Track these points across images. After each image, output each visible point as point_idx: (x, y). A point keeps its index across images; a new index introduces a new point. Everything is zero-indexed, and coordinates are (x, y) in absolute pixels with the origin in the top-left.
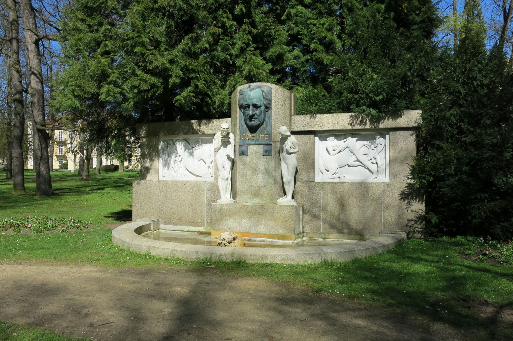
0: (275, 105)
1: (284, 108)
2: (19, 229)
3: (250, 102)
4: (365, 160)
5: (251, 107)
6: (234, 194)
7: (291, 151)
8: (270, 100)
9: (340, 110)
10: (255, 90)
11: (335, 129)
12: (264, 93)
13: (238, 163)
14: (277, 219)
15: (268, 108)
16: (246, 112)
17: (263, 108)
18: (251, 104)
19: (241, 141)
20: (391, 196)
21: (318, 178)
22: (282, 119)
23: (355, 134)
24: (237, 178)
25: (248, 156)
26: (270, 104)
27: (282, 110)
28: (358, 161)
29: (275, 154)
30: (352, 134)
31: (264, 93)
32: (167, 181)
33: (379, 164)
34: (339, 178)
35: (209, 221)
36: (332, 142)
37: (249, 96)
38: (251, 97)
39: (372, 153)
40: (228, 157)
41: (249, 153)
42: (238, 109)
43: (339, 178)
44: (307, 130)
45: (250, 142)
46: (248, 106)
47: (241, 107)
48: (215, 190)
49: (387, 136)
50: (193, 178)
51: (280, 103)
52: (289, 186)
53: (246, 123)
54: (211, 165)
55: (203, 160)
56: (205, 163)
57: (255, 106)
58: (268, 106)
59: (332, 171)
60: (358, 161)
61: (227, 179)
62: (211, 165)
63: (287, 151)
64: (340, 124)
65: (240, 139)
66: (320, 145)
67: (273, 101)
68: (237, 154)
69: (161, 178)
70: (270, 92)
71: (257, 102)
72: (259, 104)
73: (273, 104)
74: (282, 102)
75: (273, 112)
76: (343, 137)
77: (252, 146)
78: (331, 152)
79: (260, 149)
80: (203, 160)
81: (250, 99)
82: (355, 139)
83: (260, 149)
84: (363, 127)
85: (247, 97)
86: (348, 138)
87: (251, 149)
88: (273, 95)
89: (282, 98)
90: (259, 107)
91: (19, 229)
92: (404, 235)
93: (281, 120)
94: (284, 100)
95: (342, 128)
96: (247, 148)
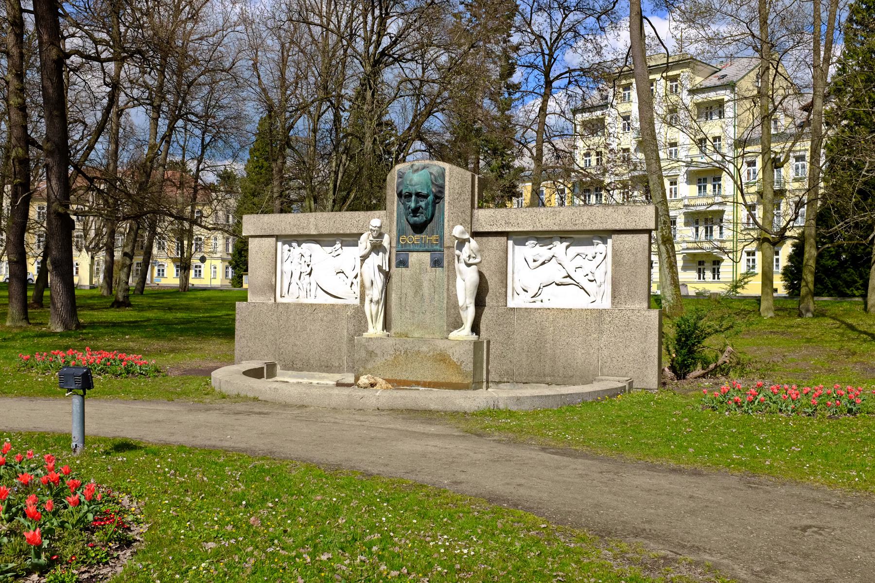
3: (412, 189)
4: (578, 276)
6: (386, 325)
11: (535, 229)
13: (394, 279)
15: (438, 197)
18: (414, 192)
19: (400, 246)
20: (612, 329)
23: (566, 238)
27: (459, 202)
28: (569, 276)
29: (448, 265)
30: (561, 238)
31: (432, 176)
32: (289, 304)
34: (542, 301)
36: (532, 250)
39: (589, 266)
40: (380, 268)
42: (396, 195)
43: (542, 301)
45: (412, 248)
47: (400, 195)
48: (360, 319)
49: (610, 241)
64: (543, 223)
65: (398, 242)
67: (447, 188)
68: (394, 263)
70: (443, 175)
71: (422, 189)
72: (425, 192)
73: (447, 192)
75: (446, 205)
76: (548, 241)
77: (415, 254)
79: (426, 257)
81: (411, 185)
82: (565, 244)
83: (426, 257)
86: (555, 243)
87: (413, 257)
88: (447, 179)
89: (460, 183)
92: (337, 364)
95: (545, 228)
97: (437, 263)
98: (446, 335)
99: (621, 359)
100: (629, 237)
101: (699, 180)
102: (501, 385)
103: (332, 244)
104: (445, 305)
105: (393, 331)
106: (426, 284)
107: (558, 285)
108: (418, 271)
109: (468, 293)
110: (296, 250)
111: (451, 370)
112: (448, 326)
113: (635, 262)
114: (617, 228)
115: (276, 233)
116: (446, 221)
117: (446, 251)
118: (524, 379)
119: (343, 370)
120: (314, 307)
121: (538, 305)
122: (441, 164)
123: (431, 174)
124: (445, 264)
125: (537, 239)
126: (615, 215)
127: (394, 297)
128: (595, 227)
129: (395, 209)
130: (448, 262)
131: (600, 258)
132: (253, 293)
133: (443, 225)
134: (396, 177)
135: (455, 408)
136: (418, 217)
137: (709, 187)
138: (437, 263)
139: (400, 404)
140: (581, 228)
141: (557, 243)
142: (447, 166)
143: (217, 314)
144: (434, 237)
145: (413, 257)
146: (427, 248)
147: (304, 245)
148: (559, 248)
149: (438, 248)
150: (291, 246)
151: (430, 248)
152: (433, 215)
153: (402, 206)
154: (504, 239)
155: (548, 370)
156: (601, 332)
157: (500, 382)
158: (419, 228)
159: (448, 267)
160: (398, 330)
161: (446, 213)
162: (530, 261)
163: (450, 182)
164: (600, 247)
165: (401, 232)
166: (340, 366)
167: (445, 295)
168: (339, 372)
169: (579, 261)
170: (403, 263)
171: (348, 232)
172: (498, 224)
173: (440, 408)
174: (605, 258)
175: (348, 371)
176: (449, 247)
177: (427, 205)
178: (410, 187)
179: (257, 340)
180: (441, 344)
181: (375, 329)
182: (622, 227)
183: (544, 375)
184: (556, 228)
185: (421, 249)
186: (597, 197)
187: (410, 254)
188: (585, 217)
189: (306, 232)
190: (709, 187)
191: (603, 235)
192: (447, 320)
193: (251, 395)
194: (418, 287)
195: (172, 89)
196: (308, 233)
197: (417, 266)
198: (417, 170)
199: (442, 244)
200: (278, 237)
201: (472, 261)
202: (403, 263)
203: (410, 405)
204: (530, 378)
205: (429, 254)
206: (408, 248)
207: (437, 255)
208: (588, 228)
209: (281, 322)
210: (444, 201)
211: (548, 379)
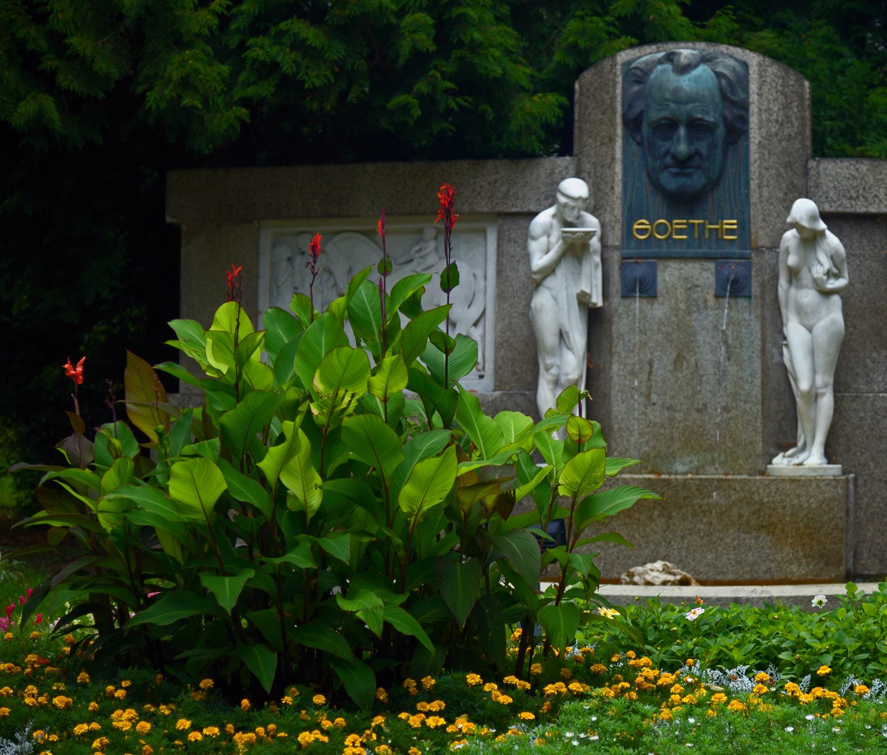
0: (761, 121)
1: (786, 133)
2: (625, 721)
5: (682, 131)
8: (744, 106)
9: (737, 42)
12: (723, 82)
13: (620, 326)
14: (780, 526)
16: (660, 143)
17: (721, 131)
22: (782, 170)
24: (615, 378)
25: (660, 299)
26: (745, 120)
27: (780, 141)
29: (763, 292)
31: (723, 82)
40: (583, 300)
41: (660, 287)
44: (863, 210)
45: (664, 250)
47: (632, 124)
51: (775, 116)
52: (565, 343)
53: (655, 184)
57: (696, 127)
58: (739, 125)
67: (753, 109)
70: (743, 81)
73: (754, 121)
74: (781, 113)
77: (673, 265)
81: (678, 102)
84: (754, 76)
85: (668, 95)
88: (753, 87)
89: (781, 99)
91: (625, 721)
93: (779, 175)
94: (786, 107)
96: (654, 268)
98: (760, 467)
108: (682, 306)
109: (821, 360)
111: (787, 549)
112: (765, 442)
116: (753, 185)
122: (738, 52)
123: (719, 75)
124: (755, 289)
129: (619, 155)
130: (762, 285)
133: (748, 196)
136: (689, 175)
142: (753, 59)
143: (609, 507)
144: (731, 223)
146: (705, 250)
151: (714, 250)
152: (722, 172)
153: (635, 148)
159: (763, 298)
161: (754, 168)
163: (760, 95)
172: (870, 197)
178: (673, 106)
185: (691, 251)
187: (661, 266)
192: (764, 427)
195: (796, 98)
197: (680, 293)
201: (833, 284)
205: (711, 265)
206: (653, 250)
207: (733, 268)
210: (747, 138)
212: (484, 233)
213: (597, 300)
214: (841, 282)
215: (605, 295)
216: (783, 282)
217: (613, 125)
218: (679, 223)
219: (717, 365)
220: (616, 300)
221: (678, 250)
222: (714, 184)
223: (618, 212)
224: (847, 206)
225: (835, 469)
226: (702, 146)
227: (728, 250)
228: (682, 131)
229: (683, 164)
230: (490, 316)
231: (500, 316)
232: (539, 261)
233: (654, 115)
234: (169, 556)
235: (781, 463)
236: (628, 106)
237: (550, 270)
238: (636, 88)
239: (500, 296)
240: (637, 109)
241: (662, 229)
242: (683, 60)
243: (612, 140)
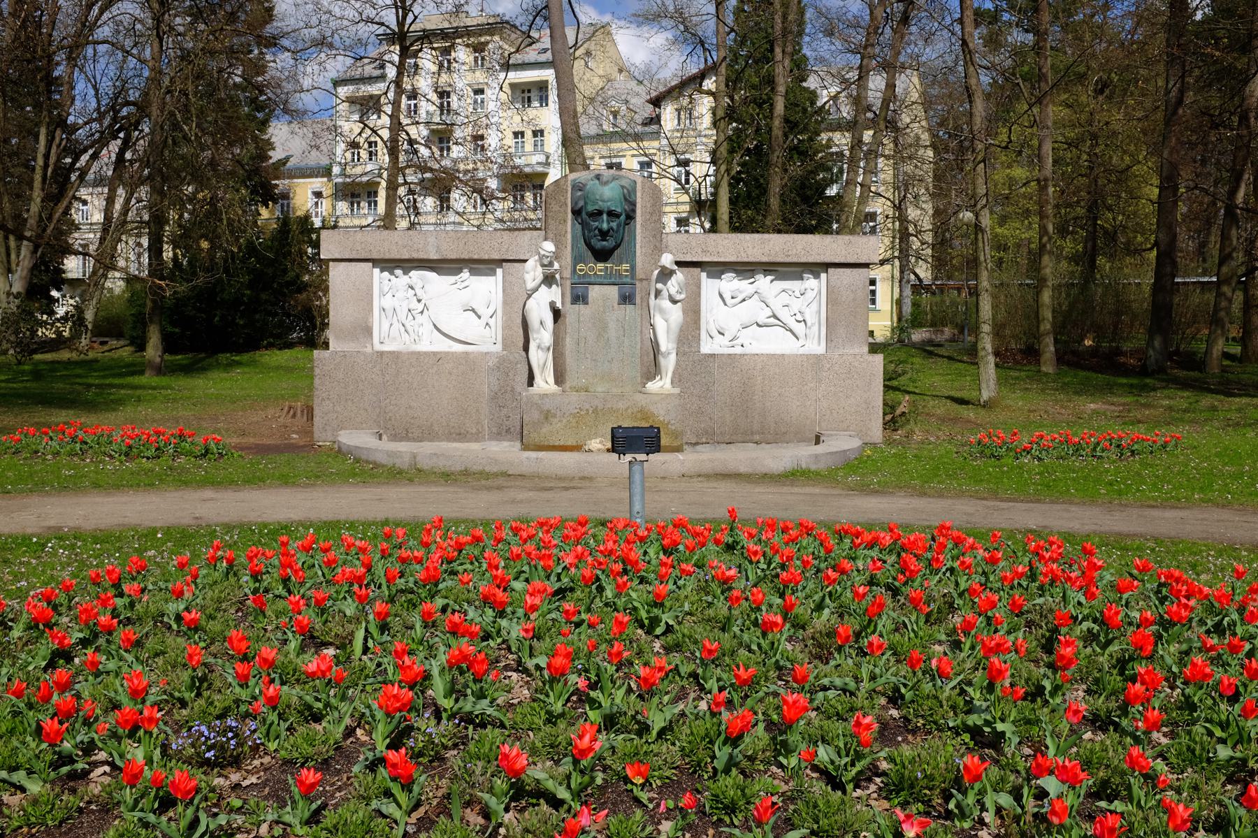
3: (604, 206)
4: (784, 315)
5: (605, 216)
6: (559, 378)
7: (678, 297)
8: (634, 204)
10: (612, 185)
11: (739, 260)
15: (630, 217)
17: (623, 217)
21: (707, 347)
26: (634, 211)
28: (775, 316)
32: (400, 353)
33: (809, 324)
35: (494, 430)
36: (730, 283)
37: (601, 195)
38: (605, 197)
39: (796, 305)
41: (590, 299)
42: (570, 215)
45: (593, 280)
46: (600, 213)
49: (823, 276)
50: (444, 345)
53: (588, 244)
54: (492, 322)
55: (473, 310)
56: (479, 317)
57: (612, 214)
59: (728, 336)
60: (775, 316)
61: (549, 349)
62: (492, 322)
63: (670, 296)
65: (574, 271)
66: (710, 287)
67: (639, 206)
68: (568, 299)
69: (378, 347)
73: (639, 212)
76: (749, 274)
77: (597, 287)
78: (729, 301)
79: (613, 292)
80: (473, 310)
81: (603, 201)
82: (770, 278)
83: (613, 292)
86: (757, 277)
87: (595, 292)
88: (639, 194)
90: (618, 216)
92: (474, 431)
95: (751, 259)
97: (626, 299)
99: (841, 411)
100: (848, 271)
101: (515, 187)
102: (699, 448)
103: (457, 271)
104: (638, 352)
105: (568, 385)
106: (612, 325)
107: (759, 326)
110: (401, 280)
113: (854, 300)
114: (837, 261)
115: (375, 256)
117: (638, 284)
118: (727, 438)
119: (483, 437)
120: (438, 357)
121: (738, 350)
123: (623, 187)
124: (638, 300)
125: (736, 271)
126: (834, 246)
127: (569, 342)
128: (811, 260)
129: (569, 229)
131: (810, 295)
132: (337, 338)
134: (570, 189)
135: (764, 470)
137: (529, 196)
138: (626, 299)
139: (707, 468)
140: (795, 260)
141: (760, 277)
144: (626, 266)
145: (595, 292)
147: (413, 273)
148: (763, 282)
149: (628, 280)
150: (392, 273)
151: (618, 280)
154: (697, 270)
155: (756, 427)
156: (820, 381)
157: (697, 444)
158: (602, 255)
160: (574, 384)
162: (727, 296)
164: (810, 283)
165: (577, 260)
166: (478, 432)
167: (638, 338)
168: (477, 440)
169: (784, 298)
170: (579, 298)
171: (486, 257)
173: (750, 471)
174: (721, 296)
175: (490, 439)
176: (641, 280)
177: (619, 226)
179: (350, 403)
180: (640, 400)
181: (545, 382)
182: (842, 260)
183: (752, 433)
184: (765, 259)
185: (606, 281)
186: (370, 205)
187: (591, 287)
188: (799, 247)
189: (422, 256)
190: (529, 196)
191: (817, 268)
193: (458, 467)
194: (602, 327)
196: (425, 257)
198: (606, 183)
199: (633, 275)
200: (375, 262)
202: (579, 298)
203: (719, 468)
204: (734, 437)
205: (616, 288)
207: (627, 289)
208: (803, 260)
209: (388, 378)
211: (757, 437)
212: (494, 274)
213: (559, 305)
214: (683, 296)
215: (563, 303)
216: (652, 296)
217: (566, 213)
218: (600, 266)
219: (618, 338)
220: (568, 305)
221: (599, 280)
222: (617, 246)
223: (569, 260)
224: (682, 258)
225: (677, 391)
226: (614, 225)
227: (625, 280)
228: (605, 216)
229: (604, 235)
230: (500, 313)
231: (504, 313)
232: (530, 285)
233: (590, 208)
234: (1154, 389)
235: (653, 386)
236: (574, 203)
237: (536, 290)
238: (579, 193)
239: (505, 303)
240: (581, 203)
241: (592, 269)
242: (605, 179)
243: (565, 221)
